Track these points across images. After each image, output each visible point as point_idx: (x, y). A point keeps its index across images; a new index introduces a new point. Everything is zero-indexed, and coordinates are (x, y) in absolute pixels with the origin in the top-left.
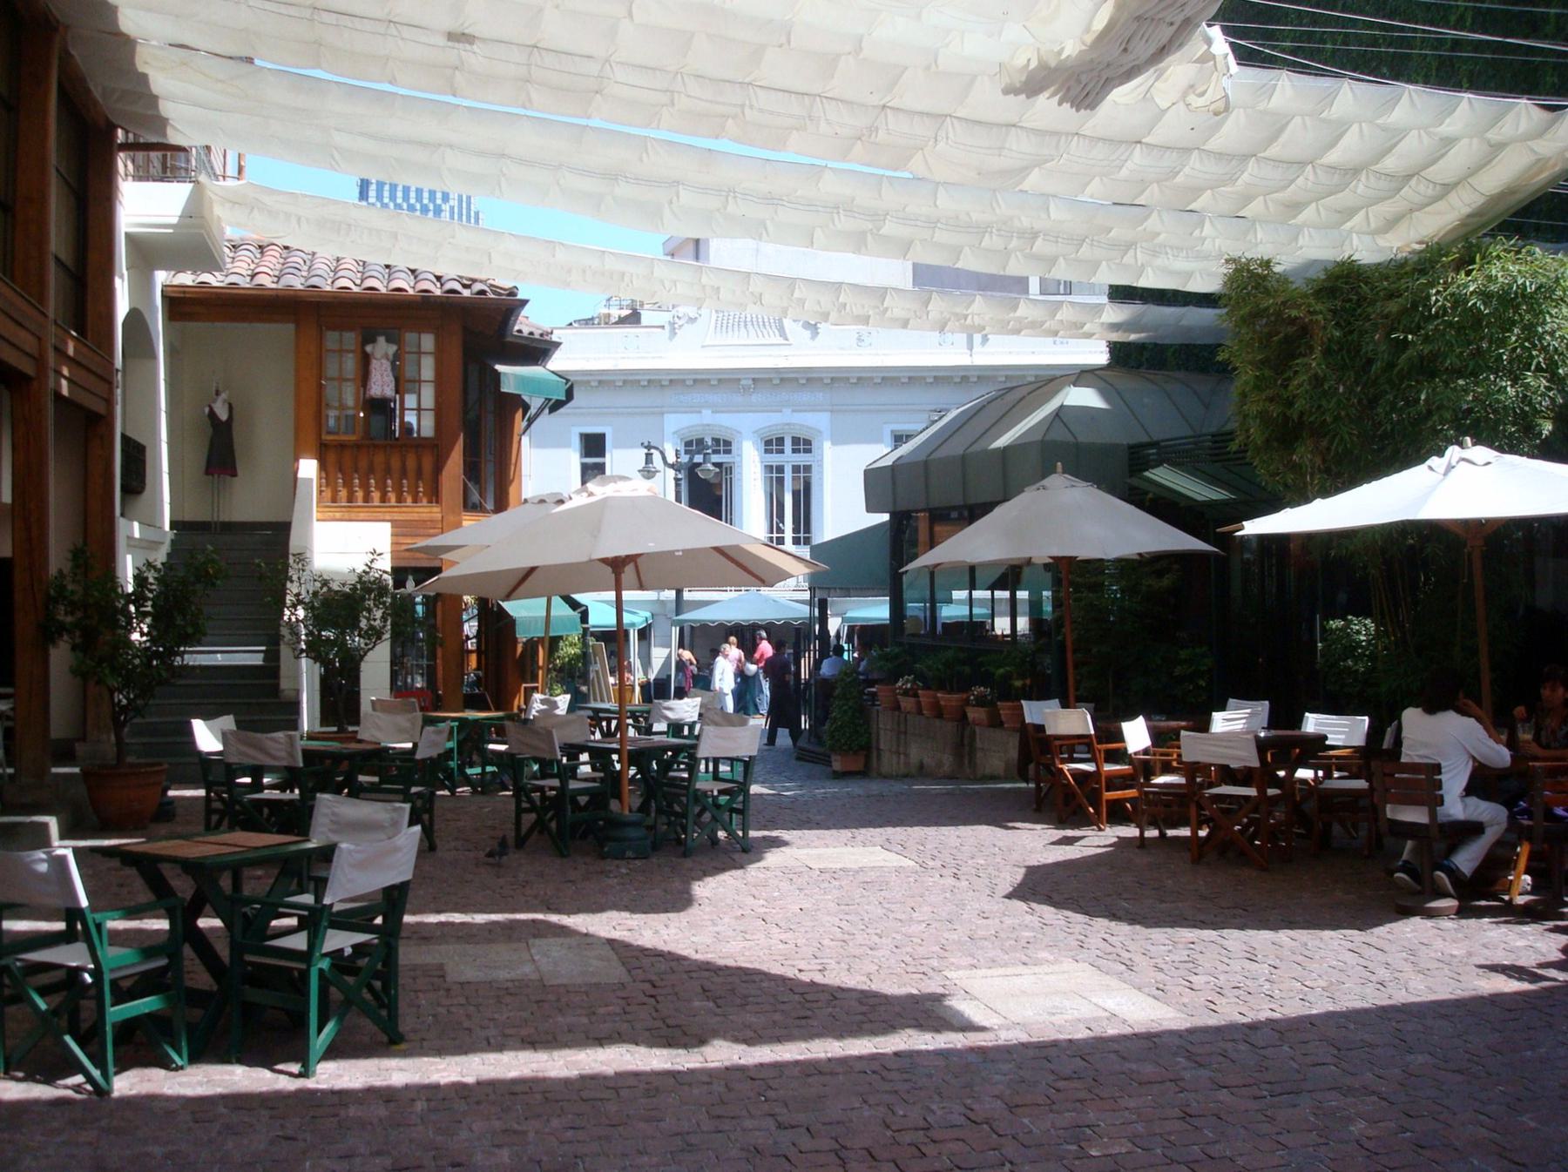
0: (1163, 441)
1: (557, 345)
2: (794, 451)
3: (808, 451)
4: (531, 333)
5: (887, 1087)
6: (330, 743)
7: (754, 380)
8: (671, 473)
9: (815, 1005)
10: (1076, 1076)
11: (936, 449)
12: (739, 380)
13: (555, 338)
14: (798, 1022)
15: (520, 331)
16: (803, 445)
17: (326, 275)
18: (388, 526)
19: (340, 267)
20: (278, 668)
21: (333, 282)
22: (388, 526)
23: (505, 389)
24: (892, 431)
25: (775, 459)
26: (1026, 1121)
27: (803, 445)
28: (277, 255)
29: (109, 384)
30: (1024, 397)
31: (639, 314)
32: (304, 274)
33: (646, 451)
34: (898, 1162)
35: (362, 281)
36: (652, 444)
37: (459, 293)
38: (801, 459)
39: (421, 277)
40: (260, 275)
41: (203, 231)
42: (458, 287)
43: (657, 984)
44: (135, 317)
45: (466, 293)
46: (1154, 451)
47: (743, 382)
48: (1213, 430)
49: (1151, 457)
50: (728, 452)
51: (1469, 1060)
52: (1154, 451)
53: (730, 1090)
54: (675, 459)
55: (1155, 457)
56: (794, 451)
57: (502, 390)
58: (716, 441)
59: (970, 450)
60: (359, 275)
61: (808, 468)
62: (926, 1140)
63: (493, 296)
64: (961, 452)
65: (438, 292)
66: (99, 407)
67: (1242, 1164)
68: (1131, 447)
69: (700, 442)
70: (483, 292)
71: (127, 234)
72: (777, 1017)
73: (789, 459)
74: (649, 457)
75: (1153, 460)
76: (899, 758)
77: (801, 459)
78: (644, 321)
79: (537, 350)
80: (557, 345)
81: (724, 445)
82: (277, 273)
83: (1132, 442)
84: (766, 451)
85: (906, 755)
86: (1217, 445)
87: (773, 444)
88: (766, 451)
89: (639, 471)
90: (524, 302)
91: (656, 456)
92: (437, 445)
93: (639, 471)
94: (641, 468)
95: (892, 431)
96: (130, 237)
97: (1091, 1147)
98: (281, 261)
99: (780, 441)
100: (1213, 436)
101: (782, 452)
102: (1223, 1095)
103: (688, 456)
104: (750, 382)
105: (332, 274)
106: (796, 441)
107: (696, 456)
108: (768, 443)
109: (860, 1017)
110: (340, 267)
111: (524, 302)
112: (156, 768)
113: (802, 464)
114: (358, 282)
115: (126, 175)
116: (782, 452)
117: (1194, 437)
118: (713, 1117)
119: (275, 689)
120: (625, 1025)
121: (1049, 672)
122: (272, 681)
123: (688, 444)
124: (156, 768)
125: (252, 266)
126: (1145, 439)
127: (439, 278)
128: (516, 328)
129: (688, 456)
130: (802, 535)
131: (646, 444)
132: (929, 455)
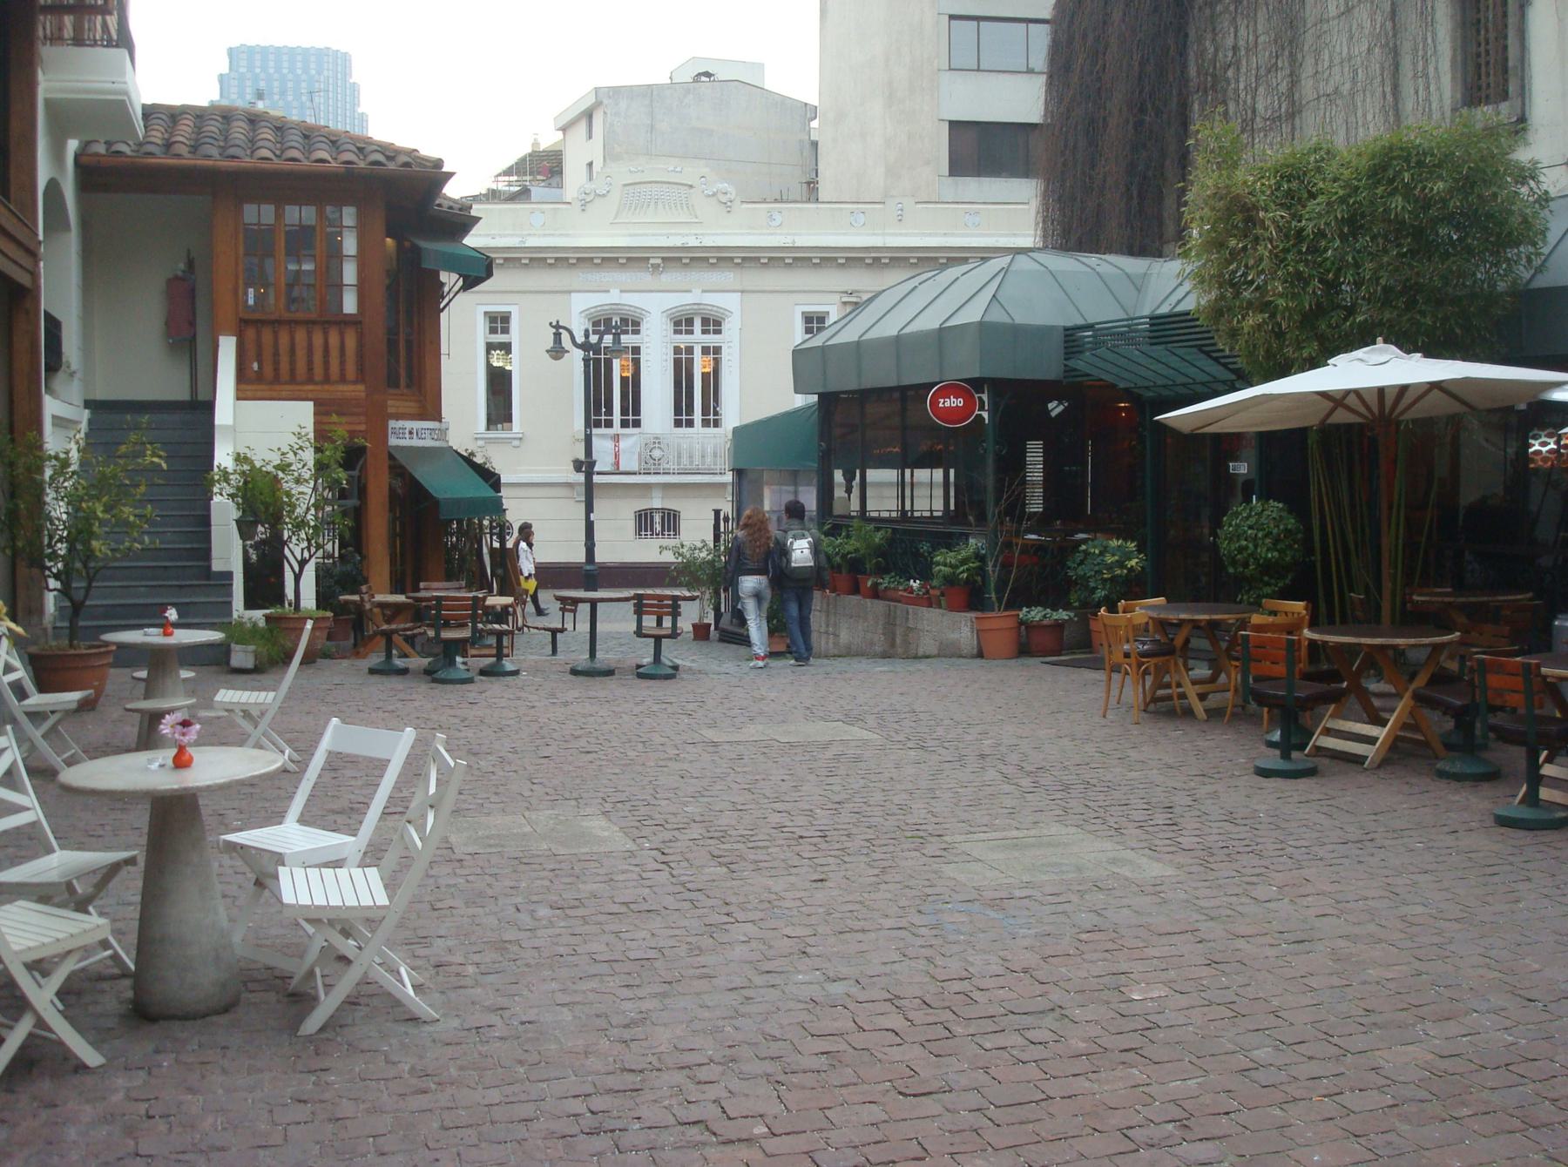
0: (1098, 324)
1: (477, 219)
2: (704, 332)
3: (718, 332)
4: (451, 208)
5: (920, 942)
6: (101, 663)
7: (663, 258)
8: (579, 354)
9: (826, 869)
10: (1095, 929)
11: (867, 331)
12: (648, 258)
13: (473, 213)
14: (814, 885)
15: (439, 205)
16: (713, 324)
17: (243, 145)
18: (311, 404)
19: (259, 138)
20: (209, 549)
21: (252, 152)
22: (311, 404)
23: (425, 265)
24: (803, 313)
25: (683, 340)
26: (1063, 970)
27: (713, 324)
28: (192, 124)
29: (33, 255)
30: (958, 278)
31: (529, 190)
32: (222, 144)
33: (554, 330)
34: (953, 1008)
35: (283, 152)
36: (561, 324)
37: (384, 165)
38: (711, 340)
39: (341, 149)
40: (176, 145)
41: (126, 98)
42: (380, 158)
43: (665, 851)
44: (53, 186)
45: (391, 166)
46: (1090, 333)
47: (652, 261)
48: (1146, 312)
49: (1087, 340)
50: (637, 332)
51: (1461, 910)
52: (1090, 333)
53: (770, 947)
54: (583, 339)
55: (1091, 339)
56: (704, 332)
57: (423, 266)
58: (624, 321)
59: (864, 338)
60: (278, 146)
61: (717, 350)
62: (972, 989)
63: (418, 169)
64: (896, 333)
65: (362, 165)
66: (24, 279)
67: (1277, 1004)
68: (1066, 329)
69: (608, 321)
70: (407, 164)
71: (47, 102)
72: (793, 879)
73: (698, 338)
74: (557, 336)
75: (1089, 343)
76: (828, 639)
77: (711, 340)
78: (534, 197)
79: (459, 221)
80: (477, 219)
81: (632, 323)
82: (192, 143)
83: (1069, 324)
84: (676, 332)
85: (836, 635)
86: (1155, 328)
87: (682, 323)
88: (676, 332)
89: (548, 351)
90: (450, 175)
91: (565, 336)
92: (360, 322)
93: (548, 351)
94: (549, 348)
95: (803, 313)
96: (47, 102)
97: (1131, 991)
98: (196, 130)
99: (690, 322)
100: (1151, 319)
101: (692, 332)
102: (1241, 943)
103: (597, 337)
104: (659, 261)
105: (250, 145)
106: (705, 321)
107: (606, 337)
108: (677, 323)
109: (874, 879)
110: (259, 138)
111: (450, 175)
112: (102, 650)
113: (712, 345)
114: (278, 153)
115: (45, 37)
116: (692, 332)
117: (1127, 320)
118: (763, 973)
119: (207, 572)
120: (647, 891)
121: (984, 552)
122: (206, 564)
123: (596, 324)
124: (102, 650)
125: (166, 136)
126: (1080, 322)
127: (361, 150)
128: (437, 202)
129: (597, 337)
130: (712, 417)
131: (554, 324)
132: (902, 329)
